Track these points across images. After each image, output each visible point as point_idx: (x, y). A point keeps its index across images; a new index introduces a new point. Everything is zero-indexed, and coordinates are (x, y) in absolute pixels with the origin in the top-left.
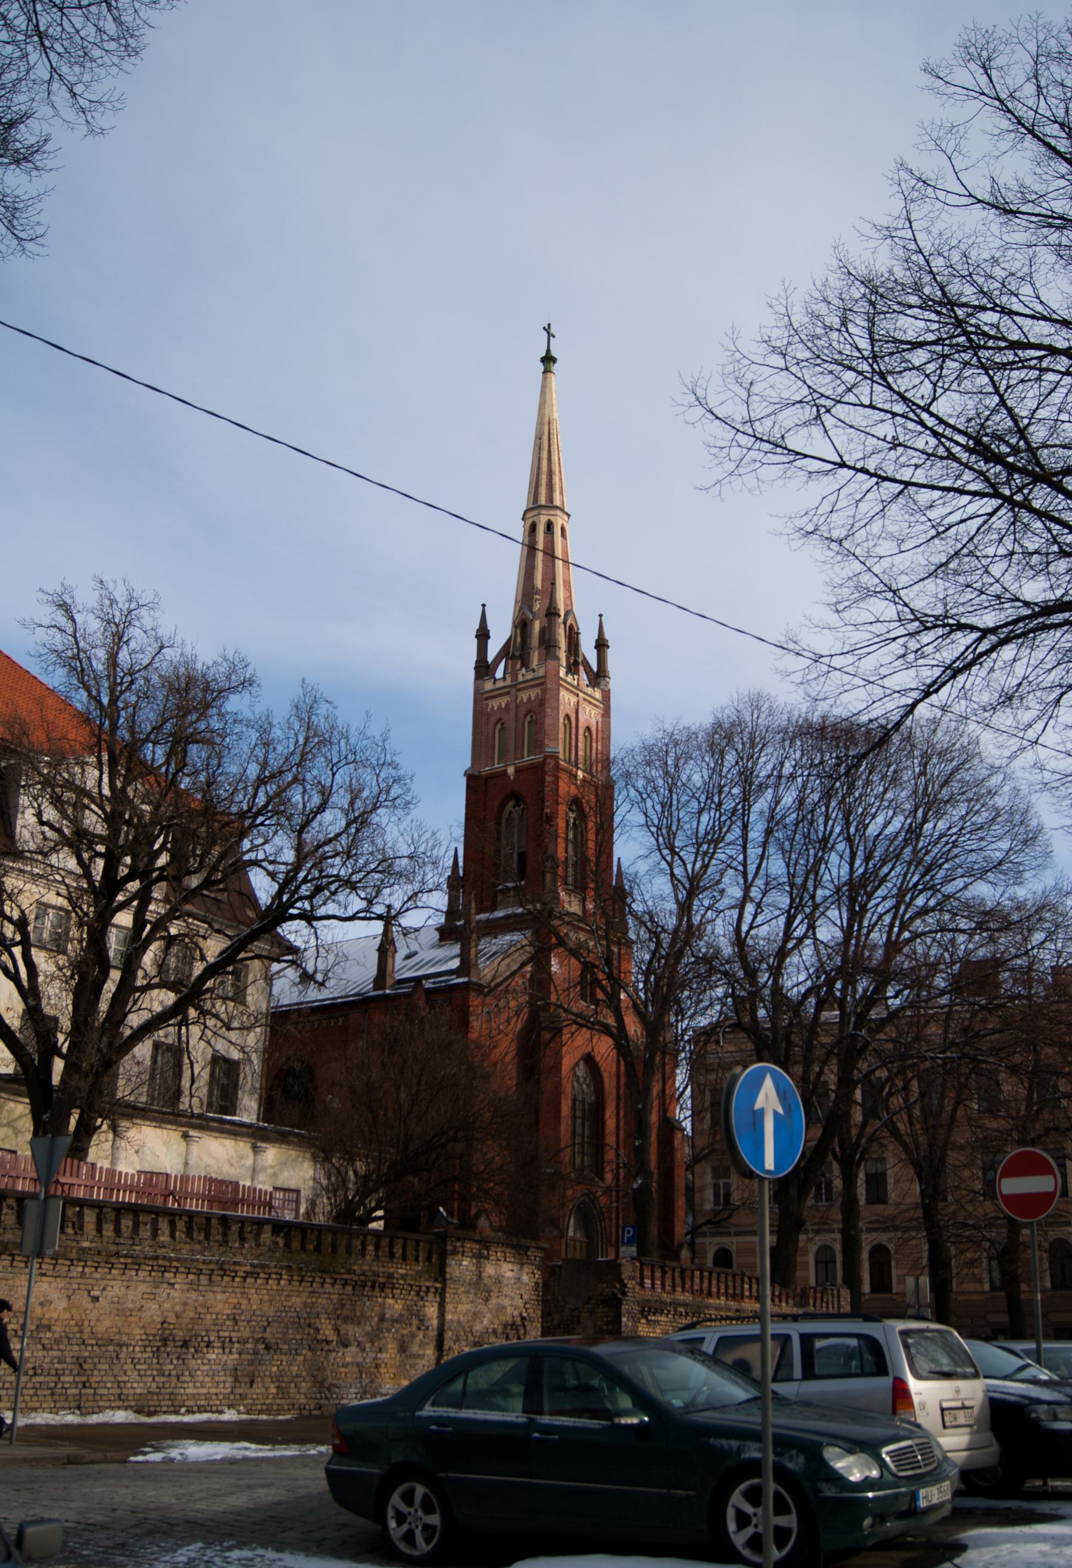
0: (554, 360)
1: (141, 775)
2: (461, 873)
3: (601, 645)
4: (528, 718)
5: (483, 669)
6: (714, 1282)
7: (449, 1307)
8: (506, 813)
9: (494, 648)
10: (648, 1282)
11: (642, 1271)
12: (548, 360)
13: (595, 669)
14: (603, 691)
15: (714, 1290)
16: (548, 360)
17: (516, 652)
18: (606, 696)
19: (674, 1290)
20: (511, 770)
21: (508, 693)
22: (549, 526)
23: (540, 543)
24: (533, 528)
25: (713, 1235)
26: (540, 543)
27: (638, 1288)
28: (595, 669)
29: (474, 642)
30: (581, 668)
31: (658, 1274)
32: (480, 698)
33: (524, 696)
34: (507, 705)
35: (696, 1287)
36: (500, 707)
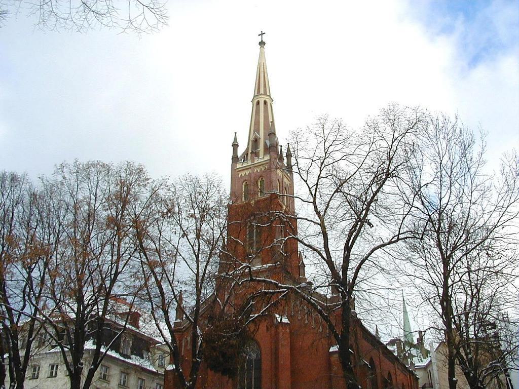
0: (264, 43)
4: (244, 183)
5: (235, 159)
9: (241, 151)
12: (262, 44)
16: (262, 44)
22: (265, 103)
23: (262, 104)
24: (258, 103)
26: (262, 104)
32: (233, 170)
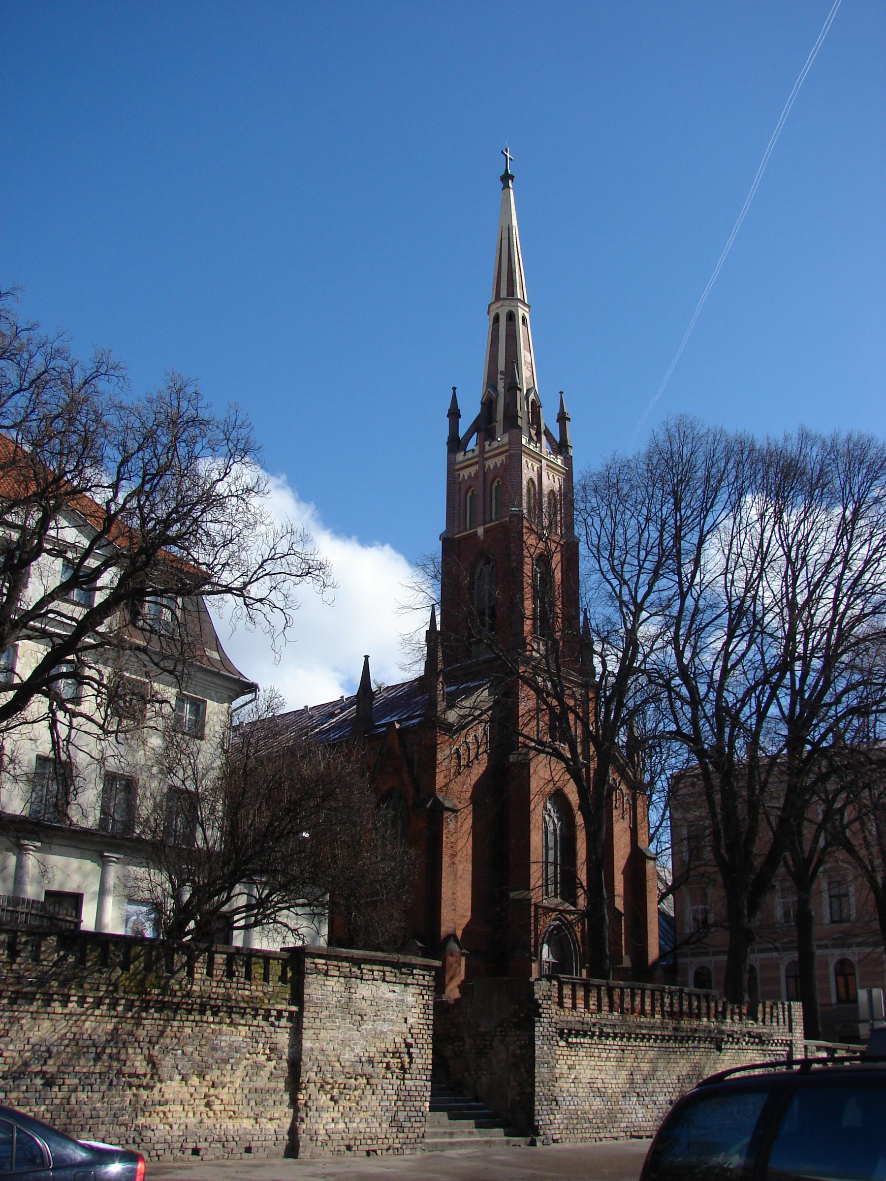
2: (438, 628)
3: (562, 418)
5: (455, 444)
6: (648, 1001)
7: (307, 1034)
8: (478, 570)
9: (464, 425)
10: (568, 1002)
11: (560, 990)
13: (558, 440)
14: (565, 458)
15: (648, 1007)
17: (484, 426)
18: (568, 461)
19: (599, 1010)
24: (496, 319)
25: (694, 955)
27: (555, 1007)
29: (446, 421)
30: (544, 438)
31: (580, 993)
33: (490, 464)
35: (667, 1008)
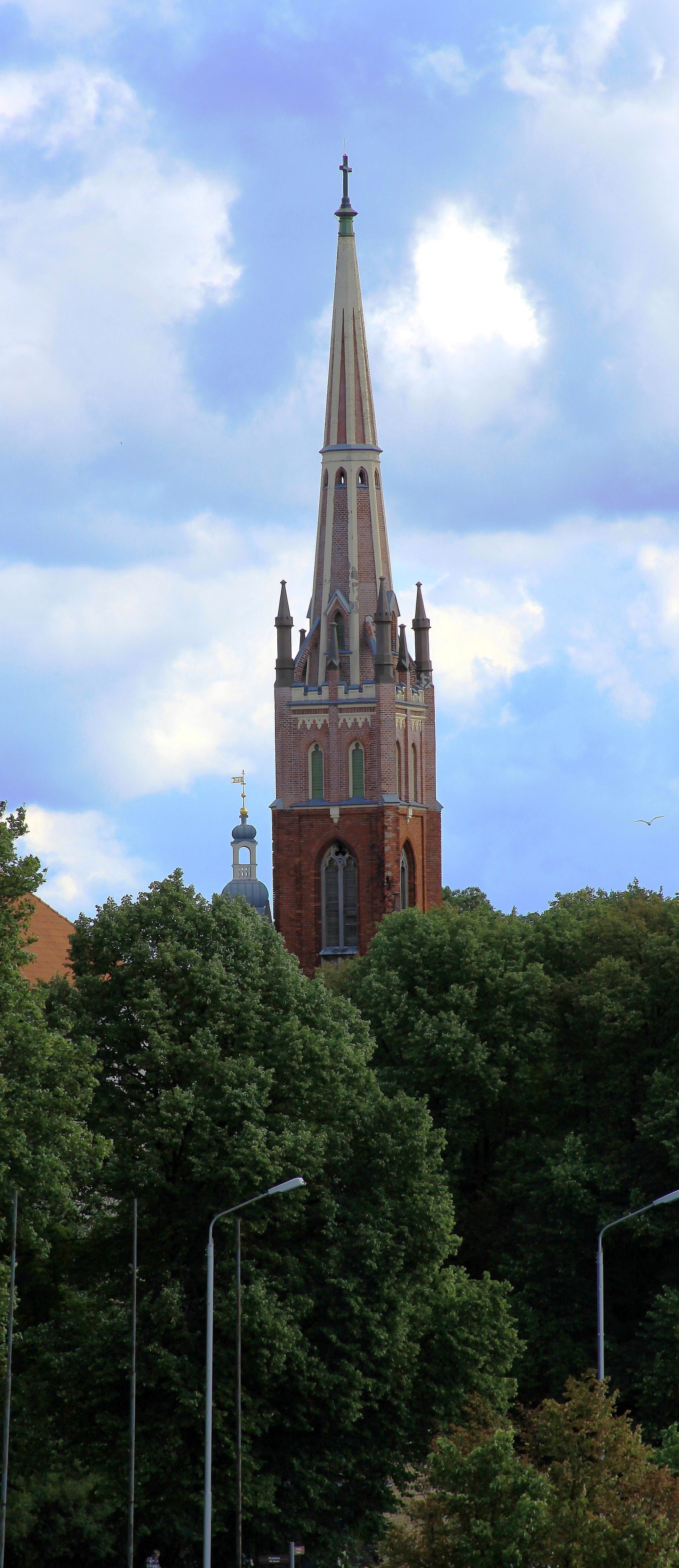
1: (74, 1041)
3: (421, 626)
8: (326, 860)
12: (346, 215)
20: (335, 812)
21: (326, 711)
22: (362, 474)
24: (342, 473)
28: (414, 659)
29: (273, 633)
34: (325, 725)
36: (314, 725)
